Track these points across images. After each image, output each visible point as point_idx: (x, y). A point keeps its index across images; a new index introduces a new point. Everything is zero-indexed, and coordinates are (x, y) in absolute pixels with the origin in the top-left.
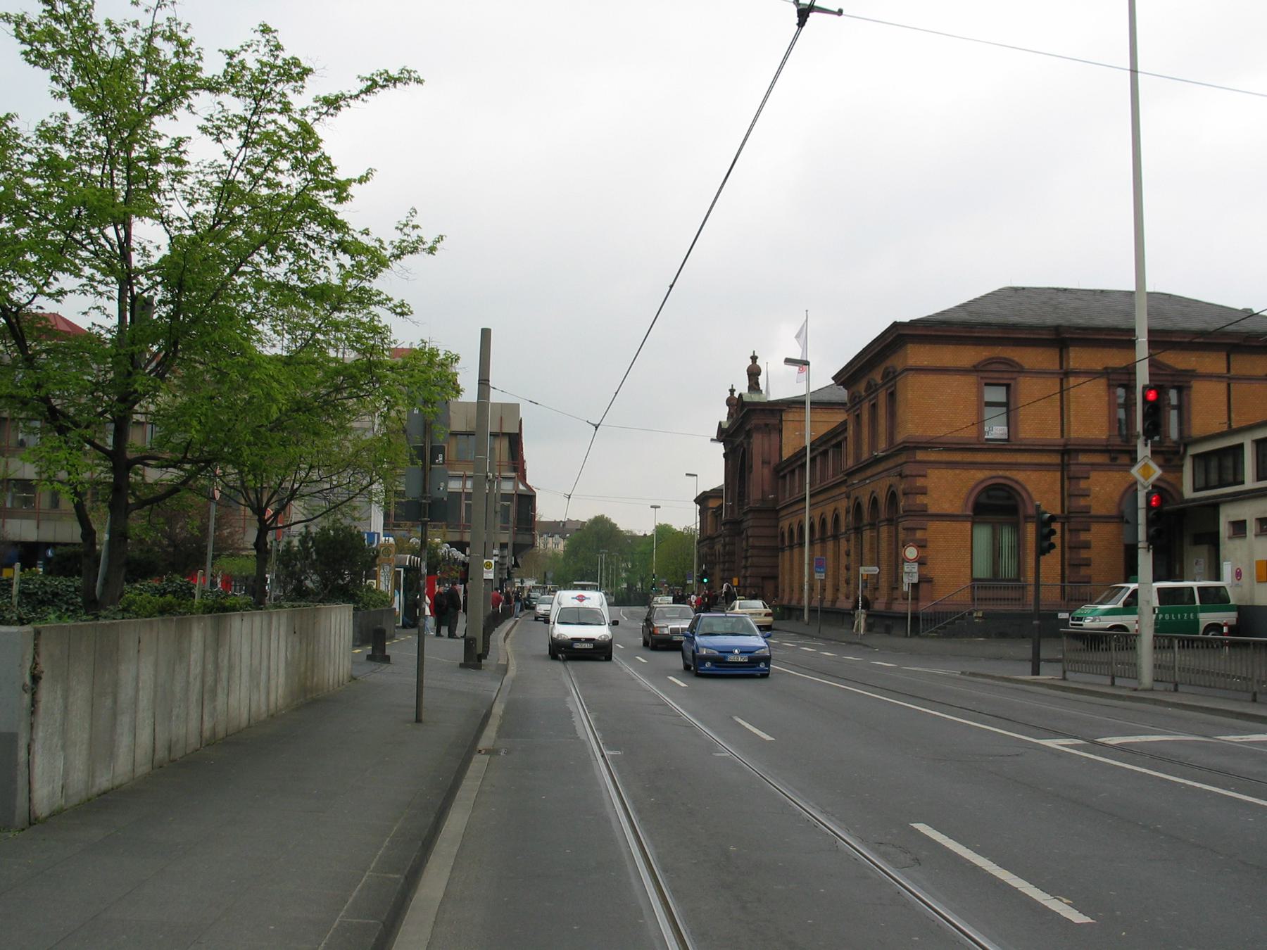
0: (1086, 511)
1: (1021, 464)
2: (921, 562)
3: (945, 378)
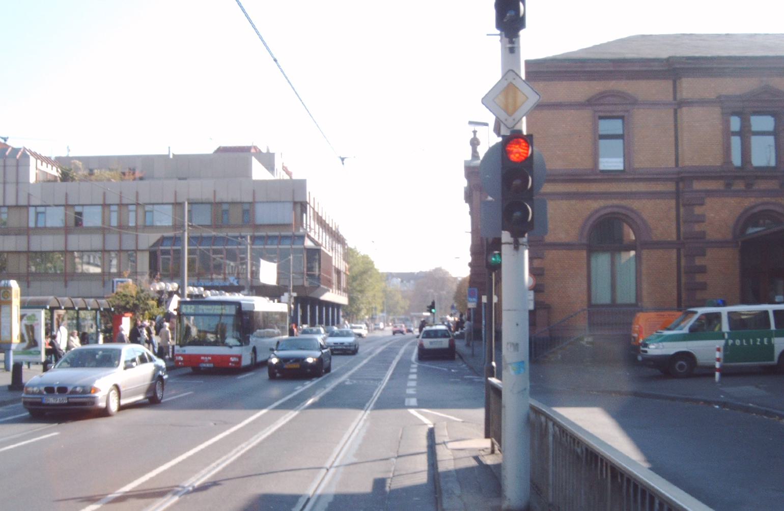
1: (592, 194)
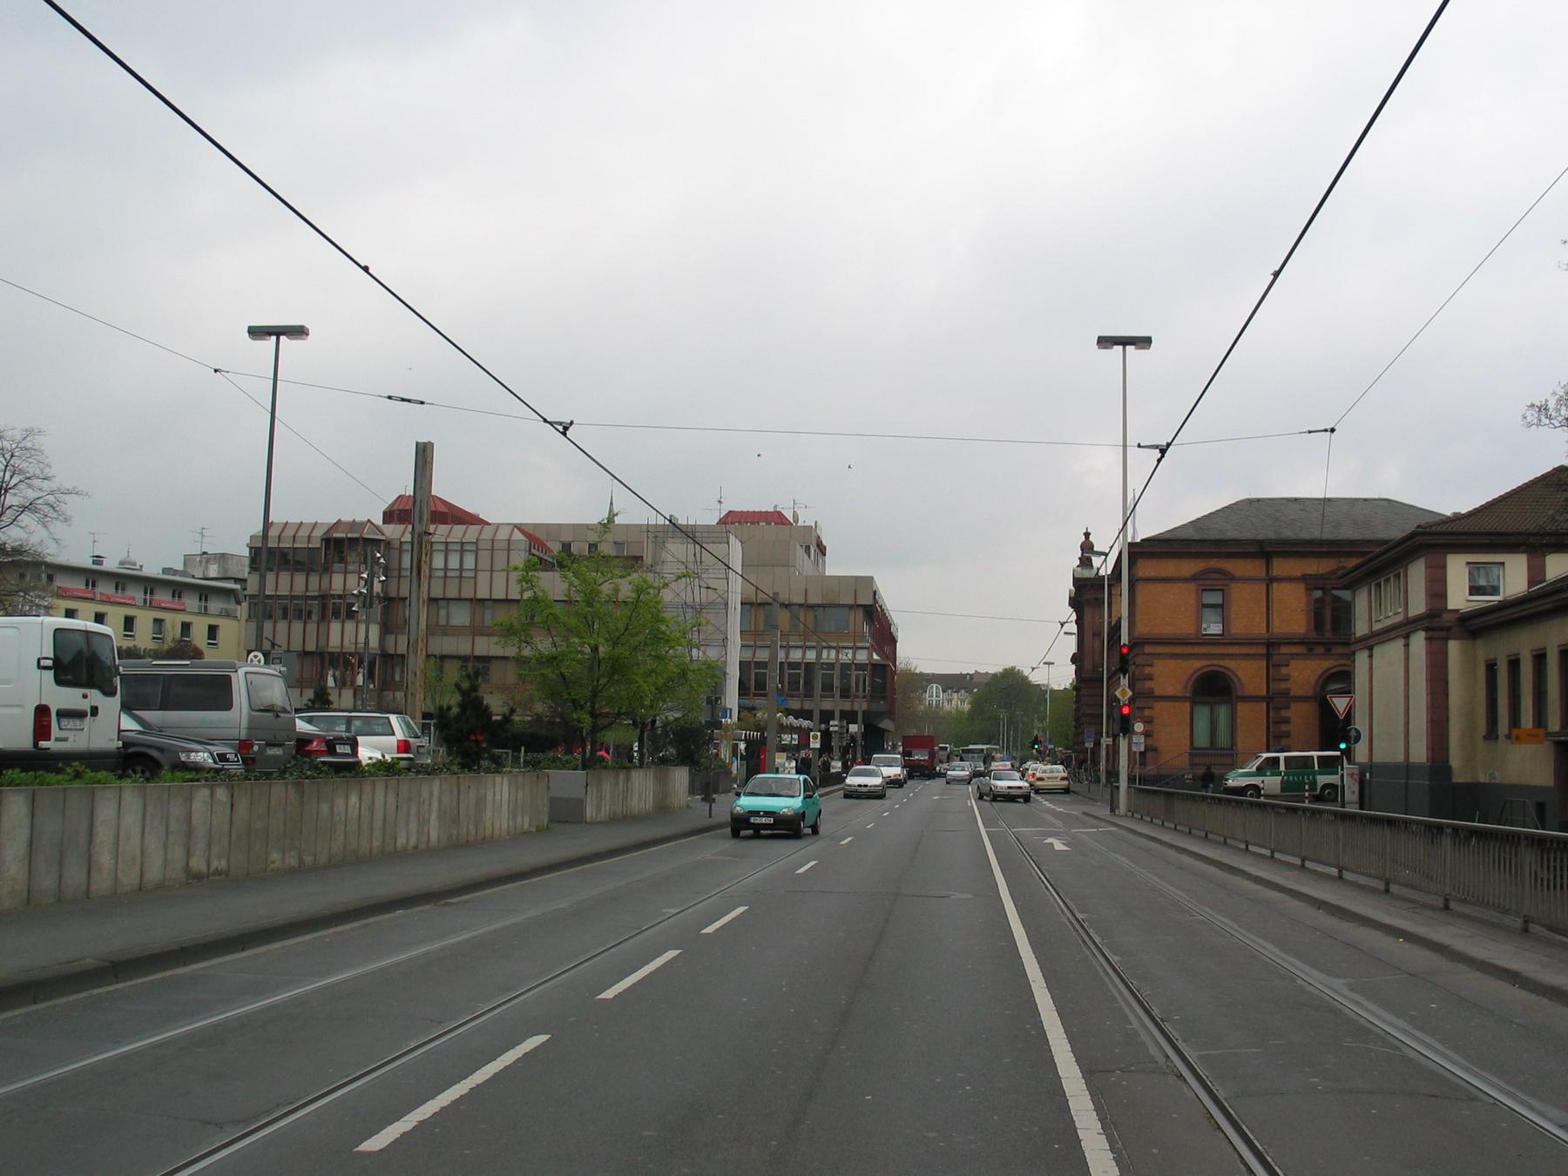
0: (1286, 694)
2: (1147, 734)
3: (1168, 586)
